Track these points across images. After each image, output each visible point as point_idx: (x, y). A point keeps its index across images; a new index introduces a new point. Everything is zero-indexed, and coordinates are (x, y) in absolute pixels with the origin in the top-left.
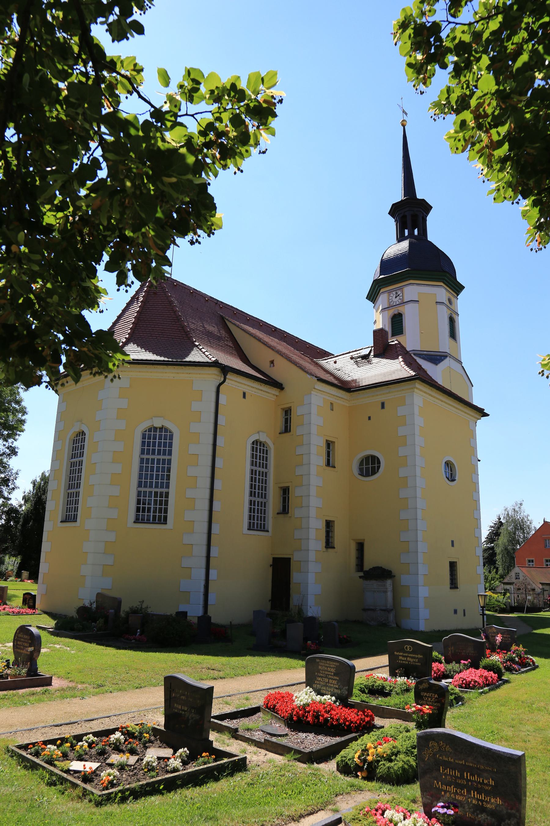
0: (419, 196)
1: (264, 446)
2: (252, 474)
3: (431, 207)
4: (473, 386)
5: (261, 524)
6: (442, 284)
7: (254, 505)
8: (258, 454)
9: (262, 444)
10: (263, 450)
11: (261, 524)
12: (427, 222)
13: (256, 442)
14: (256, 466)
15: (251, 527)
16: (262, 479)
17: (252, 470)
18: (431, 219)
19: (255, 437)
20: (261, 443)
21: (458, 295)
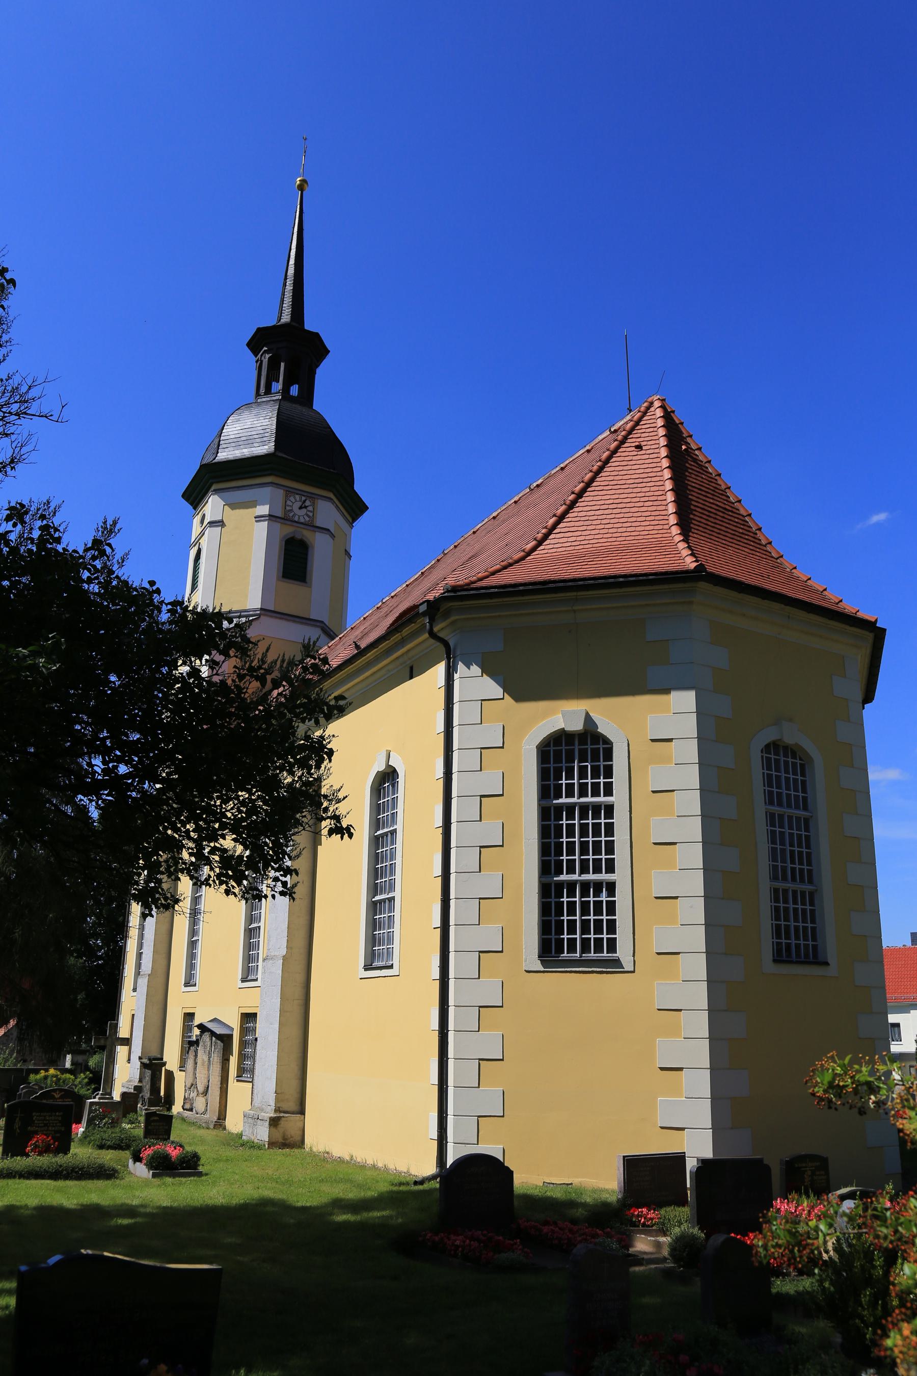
0: (308, 326)
1: (794, 757)
2: (777, 900)
3: (328, 352)
4: (350, 557)
5: (806, 946)
6: (331, 495)
7: (786, 901)
8: (791, 906)
9: (791, 751)
10: (794, 764)
11: (806, 946)
12: (316, 376)
13: (773, 747)
14: (784, 879)
15: (782, 956)
16: (800, 853)
17: (776, 891)
18: (323, 374)
19: (769, 735)
20: (786, 748)
21: (354, 520)
